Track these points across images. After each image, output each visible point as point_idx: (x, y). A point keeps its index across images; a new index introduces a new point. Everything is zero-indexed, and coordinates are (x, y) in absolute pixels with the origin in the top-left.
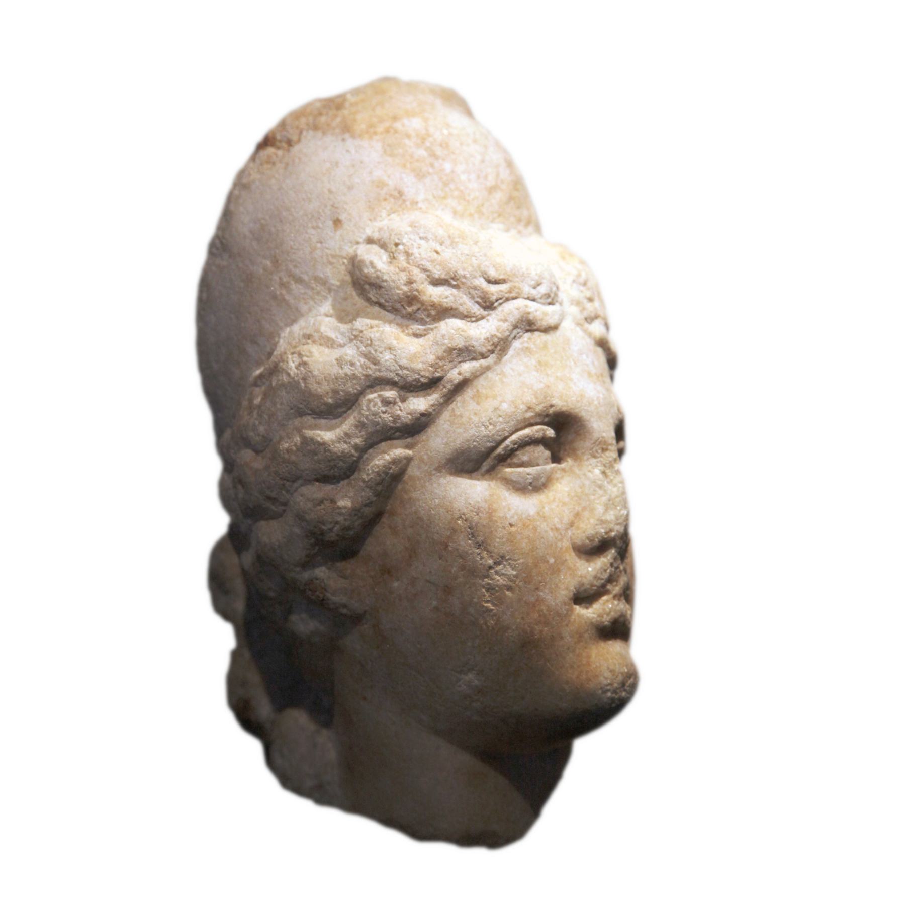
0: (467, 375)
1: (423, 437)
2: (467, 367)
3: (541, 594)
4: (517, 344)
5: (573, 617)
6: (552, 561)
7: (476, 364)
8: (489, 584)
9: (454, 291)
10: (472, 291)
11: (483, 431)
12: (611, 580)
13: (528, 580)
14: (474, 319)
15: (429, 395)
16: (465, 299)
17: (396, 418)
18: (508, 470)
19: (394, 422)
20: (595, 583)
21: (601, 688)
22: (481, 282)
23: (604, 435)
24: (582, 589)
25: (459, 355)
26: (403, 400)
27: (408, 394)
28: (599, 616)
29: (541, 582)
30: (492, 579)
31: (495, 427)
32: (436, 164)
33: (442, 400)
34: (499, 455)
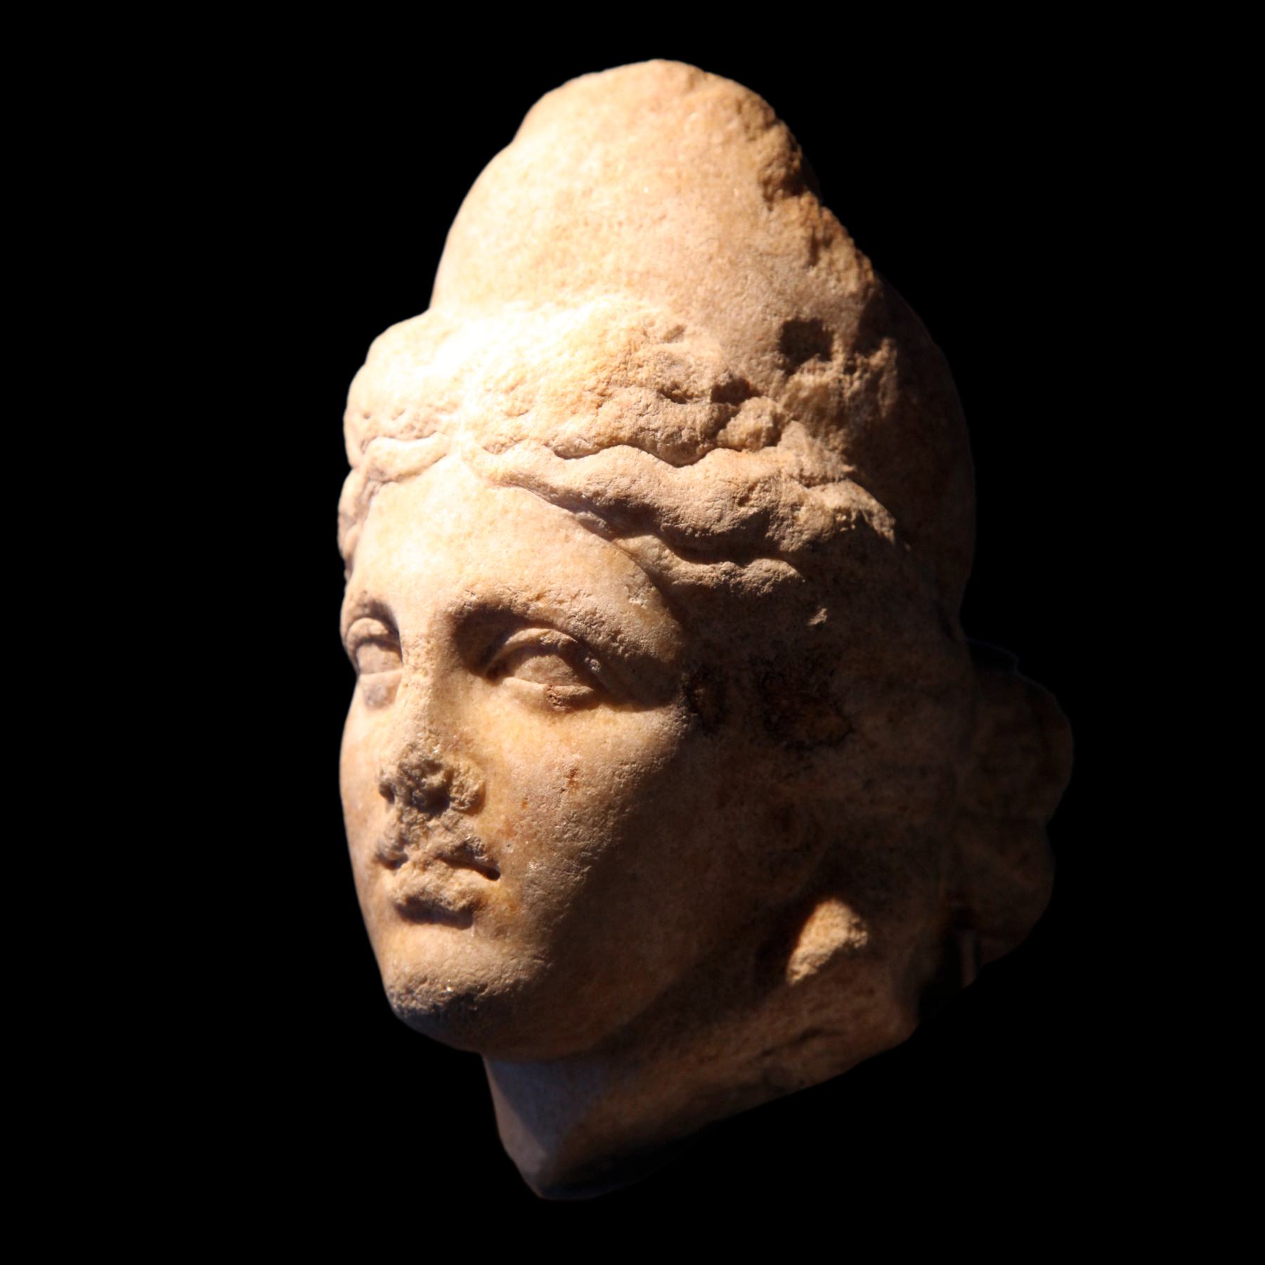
12: (402, 841)
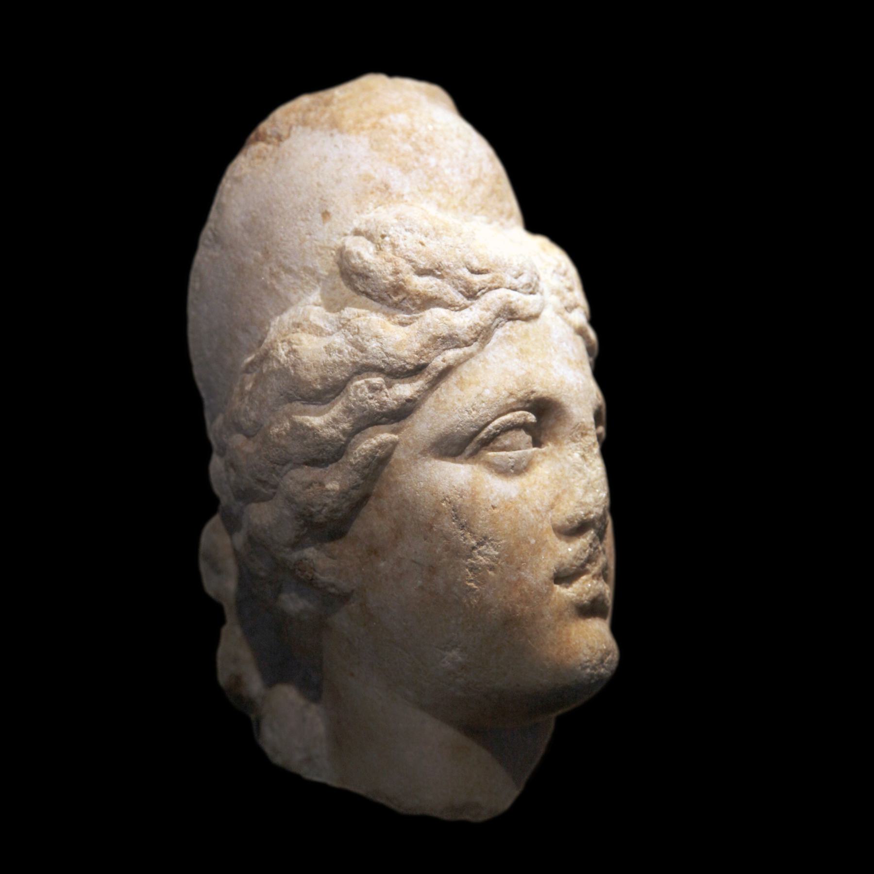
0: (451, 362)
1: (409, 422)
2: (451, 355)
3: (523, 573)
4: (499, 333)
5: (553, 596)
6: (533, 541)
7: (459, 352)
8: (472, 564)
9: (439, 281)
10: (456, 281)
11: (467, 416)
13: (510, 560)
14: (457, 308)
15: (415, 381)
16: (449, 288)
17: (383, 404)
18: (491, 454)
19: (381, 407)
20: (575, 563)
21: (581, 665)
22: (465, 273)
23: (584, 420)
24: (562, 568)
25: (443, 343)
26: (390, 386)
27: (394, 381)
28: (578, 595)
29: (522, 562)
30: (475, 559)
31: (478, 412)
32: (421, 159)
33: (426, 387)
34: (482, 439)
